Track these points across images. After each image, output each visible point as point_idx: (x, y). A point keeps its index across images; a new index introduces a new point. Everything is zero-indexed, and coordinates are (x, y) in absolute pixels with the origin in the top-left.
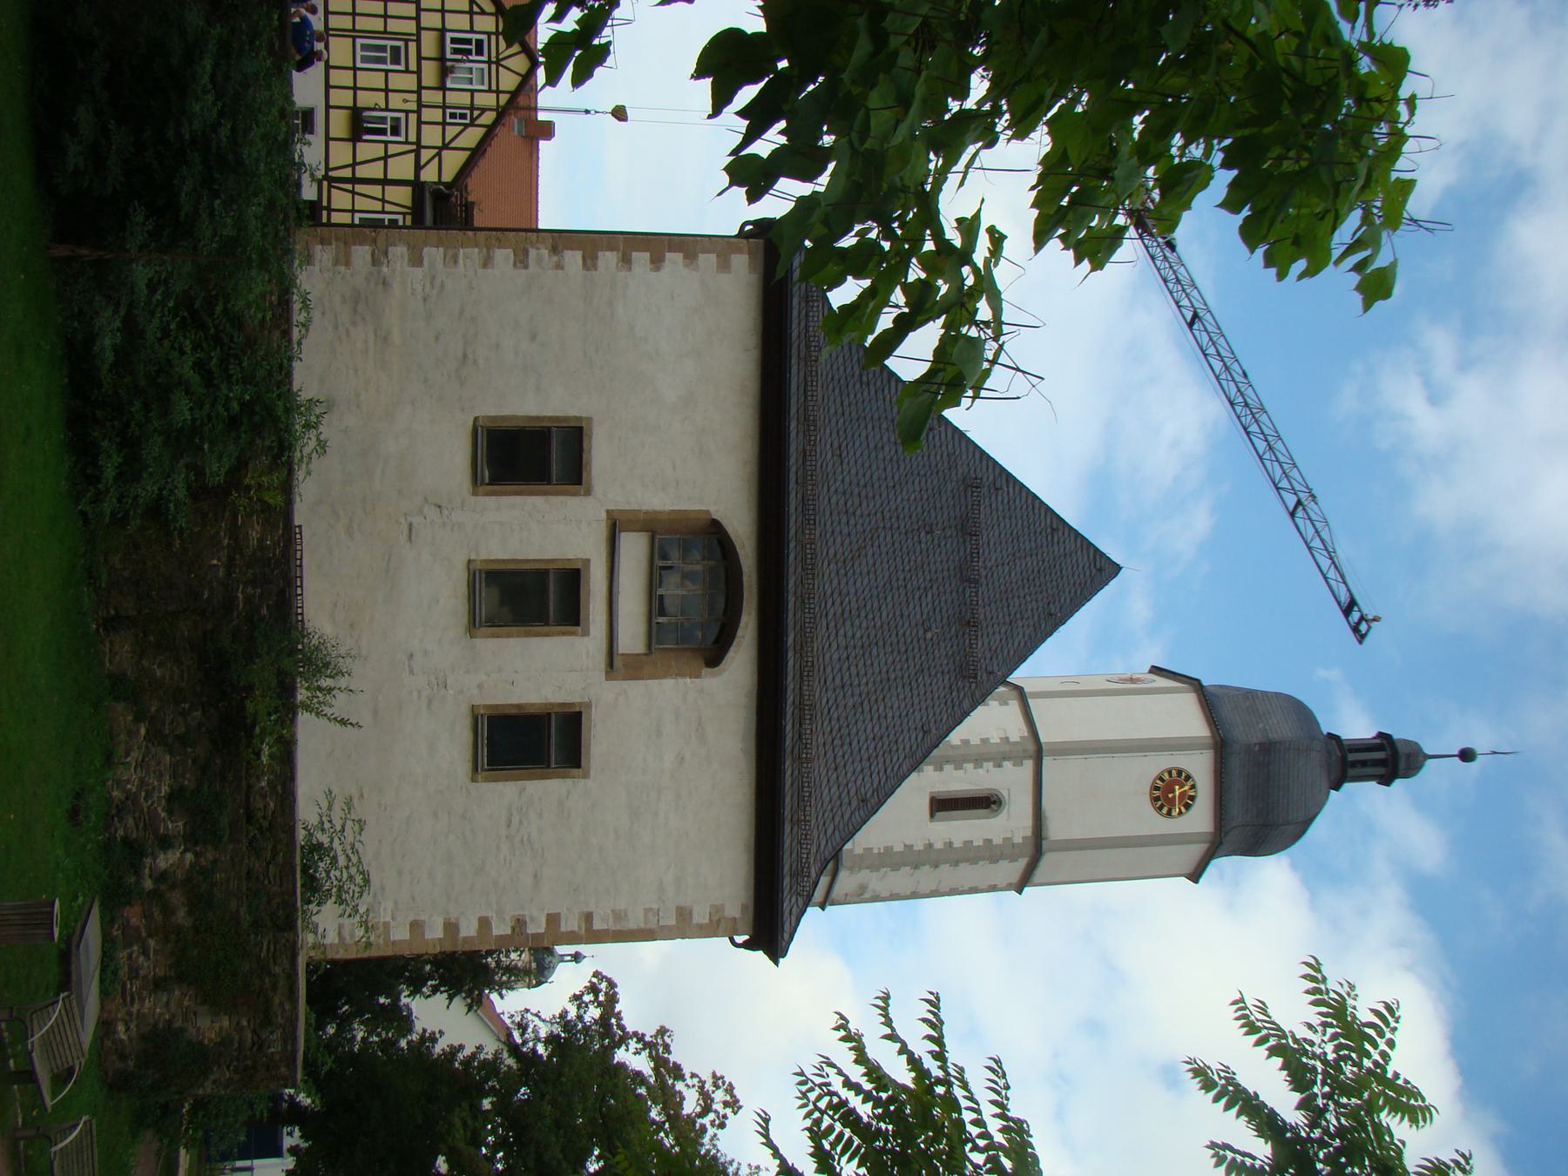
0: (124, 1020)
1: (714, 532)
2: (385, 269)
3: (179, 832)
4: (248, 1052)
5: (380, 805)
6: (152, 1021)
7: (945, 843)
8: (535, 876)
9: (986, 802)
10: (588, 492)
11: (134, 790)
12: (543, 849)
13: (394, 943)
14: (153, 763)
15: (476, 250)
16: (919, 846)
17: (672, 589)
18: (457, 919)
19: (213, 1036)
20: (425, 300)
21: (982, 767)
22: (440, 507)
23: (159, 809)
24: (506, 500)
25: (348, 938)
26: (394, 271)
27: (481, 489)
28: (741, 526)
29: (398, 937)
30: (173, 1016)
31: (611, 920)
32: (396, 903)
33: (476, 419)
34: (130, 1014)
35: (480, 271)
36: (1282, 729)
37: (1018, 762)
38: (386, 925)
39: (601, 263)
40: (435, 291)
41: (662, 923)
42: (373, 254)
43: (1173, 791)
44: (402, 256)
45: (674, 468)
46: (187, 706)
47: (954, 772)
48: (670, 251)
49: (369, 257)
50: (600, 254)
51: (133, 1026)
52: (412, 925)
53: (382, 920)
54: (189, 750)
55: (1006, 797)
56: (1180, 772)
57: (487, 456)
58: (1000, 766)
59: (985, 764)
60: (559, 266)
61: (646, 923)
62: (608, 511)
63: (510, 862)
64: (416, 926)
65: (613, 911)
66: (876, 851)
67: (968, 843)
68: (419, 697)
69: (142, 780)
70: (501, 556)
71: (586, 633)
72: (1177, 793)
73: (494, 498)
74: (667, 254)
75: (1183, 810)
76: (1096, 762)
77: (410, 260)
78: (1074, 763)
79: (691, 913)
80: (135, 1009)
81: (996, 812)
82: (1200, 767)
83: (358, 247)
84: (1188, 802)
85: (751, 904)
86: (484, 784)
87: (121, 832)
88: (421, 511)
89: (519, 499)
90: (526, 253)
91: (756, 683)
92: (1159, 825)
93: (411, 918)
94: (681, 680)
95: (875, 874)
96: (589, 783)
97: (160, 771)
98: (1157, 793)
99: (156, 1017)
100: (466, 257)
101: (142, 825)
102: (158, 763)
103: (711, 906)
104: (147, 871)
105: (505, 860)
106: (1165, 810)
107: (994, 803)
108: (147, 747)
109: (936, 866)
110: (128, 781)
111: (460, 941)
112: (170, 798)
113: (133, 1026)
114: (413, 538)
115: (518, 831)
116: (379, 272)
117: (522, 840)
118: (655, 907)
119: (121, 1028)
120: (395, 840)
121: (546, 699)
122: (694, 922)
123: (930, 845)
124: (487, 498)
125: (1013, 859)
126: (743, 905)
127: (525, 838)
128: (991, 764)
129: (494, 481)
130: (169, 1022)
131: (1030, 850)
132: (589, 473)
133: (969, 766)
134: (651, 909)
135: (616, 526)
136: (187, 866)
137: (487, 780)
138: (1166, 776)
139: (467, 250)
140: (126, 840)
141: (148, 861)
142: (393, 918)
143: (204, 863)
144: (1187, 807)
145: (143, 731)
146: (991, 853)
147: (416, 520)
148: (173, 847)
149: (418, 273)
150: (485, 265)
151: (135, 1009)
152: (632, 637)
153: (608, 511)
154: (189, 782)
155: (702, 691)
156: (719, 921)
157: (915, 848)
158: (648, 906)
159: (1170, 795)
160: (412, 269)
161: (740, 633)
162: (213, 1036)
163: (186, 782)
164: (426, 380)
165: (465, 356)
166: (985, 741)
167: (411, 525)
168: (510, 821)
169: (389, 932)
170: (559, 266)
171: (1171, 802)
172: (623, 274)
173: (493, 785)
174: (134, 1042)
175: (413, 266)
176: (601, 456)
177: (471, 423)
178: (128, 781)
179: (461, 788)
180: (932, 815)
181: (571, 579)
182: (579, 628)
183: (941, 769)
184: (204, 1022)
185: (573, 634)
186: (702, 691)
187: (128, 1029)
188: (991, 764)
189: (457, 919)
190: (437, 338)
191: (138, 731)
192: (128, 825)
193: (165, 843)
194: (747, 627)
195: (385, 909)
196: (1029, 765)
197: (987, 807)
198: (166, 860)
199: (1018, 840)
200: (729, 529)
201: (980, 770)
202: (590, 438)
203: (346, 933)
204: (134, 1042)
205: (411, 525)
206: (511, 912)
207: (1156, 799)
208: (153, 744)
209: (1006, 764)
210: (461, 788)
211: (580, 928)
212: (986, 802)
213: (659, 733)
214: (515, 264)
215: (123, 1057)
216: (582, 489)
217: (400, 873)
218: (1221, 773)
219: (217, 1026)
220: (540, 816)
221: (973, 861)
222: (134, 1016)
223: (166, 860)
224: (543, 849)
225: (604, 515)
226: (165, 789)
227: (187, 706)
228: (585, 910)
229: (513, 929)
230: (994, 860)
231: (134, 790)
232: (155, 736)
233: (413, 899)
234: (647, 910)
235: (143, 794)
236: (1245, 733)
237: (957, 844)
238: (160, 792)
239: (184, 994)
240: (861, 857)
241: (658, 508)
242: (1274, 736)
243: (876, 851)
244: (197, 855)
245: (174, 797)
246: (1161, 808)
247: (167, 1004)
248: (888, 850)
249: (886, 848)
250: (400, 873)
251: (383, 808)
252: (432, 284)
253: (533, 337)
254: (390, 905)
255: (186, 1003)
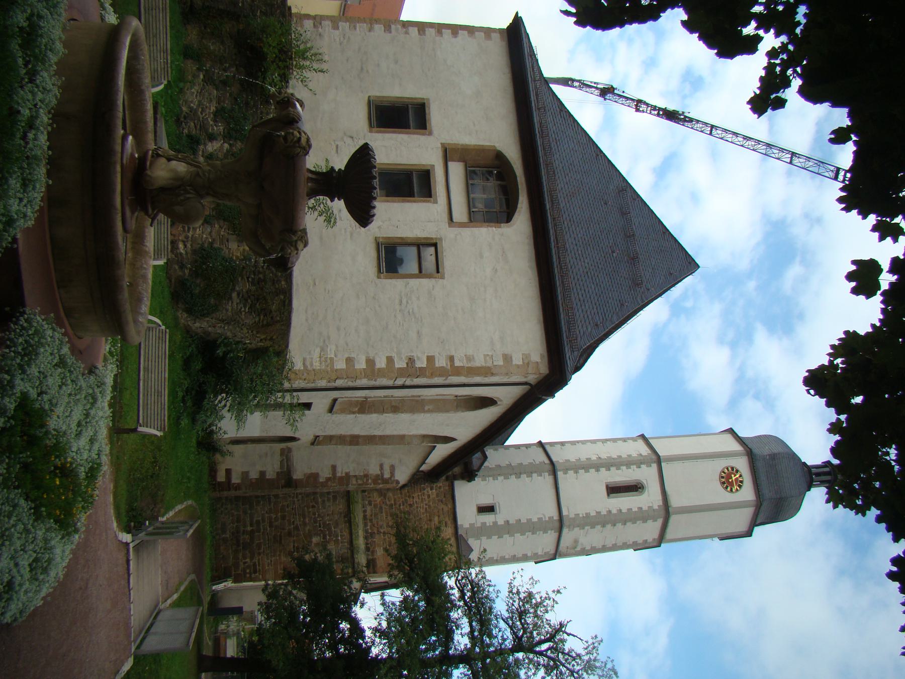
0: (184, 242)
1: (500, 157)
2: (320, 30)
3: (220, 132)
4: (261, 269)
5: (325, 289)
6: (201, 243)
7: (618, 510)
8: (418, 333)
9: (635, 488)
10: (430, 134)
11: (195, 107)
12: (421, 317)
13: (336, 370)
14: (206, 94)
15: (365, 24)
16: (604, 512)
17: (478, 195)
18: (374, 357)
19: (239, 255)
20: (341, 44)
21: (630, 468)
22: (352, 138)
23: (209, 119)
24: (387, 135)
25: (309, 367)
26: (325, 31)
27: (374, 129)
28: (513, 153)
29: (339, 367)
30: (214, 240)
31: (465, 361)
32: (337, 346)
33: (369, 97)
34: (187, 237)
35: (367, 33)
36: (777, 449)
37: (649, 465)
38: (331, 359)
39: (427, 32)
40: (345, 41)
41: (495, 363)
42: (314, 24)
43: (731, 478)
44: (329, 25)
45: (474, 125)
46: (227, 65)
47: (617, 471)
48: (461, 30)
49: (312, 25)
50: (427, 29)
51: (189, 245)
52: (347, 360)
53: (329, 356)
54: (228, 89)
55: (645, 483)
56: (732, 469)
57: (376, 121)
58: (640, 467)
59: (632, 466)
60: (407, 33)
61: (486, 363)
62: (441, 144)
63: (403, 325)
64: (349, 361)
65: (465, 355)
66: (581, 516)
67: (630, 510)
68: (345, 232)
69: (199, 102)
70: (386, 162)
71: (436, 202)
72: (734, 478)
73: (380, 134)
74: (460, 31)
75: (738, 489)
76: (688, 464)
77: (332, 27)
78: (677, 465)
79: (511, 358)
80: (190, 234)
81: (642, 493)
82: (742, 464)
83: (307, 21)
84: (740, 484)
85: (546, 354)
86: (384, 280)
87: (186, 131)
88: (342, 139)
89: (394, 136)
90: (390, 26)
91: (532, 231)
92: (726, 497)
93: (347, 356)
94: (490, 229)
95: (582, 531)
96: (445, 281)
97: (211, 98)
98: (723, 480)
99: (203, 240)
100: (360, 27)
101: (198, 127)
102: (210, 94)
103: (523, 354)
104: (201, 153)
105: (400, 323)
106: (729, 489)
107: (640, 488)
108: (203, 85)
109: (615, 525)
110: (192, 102)
111: (376, 370)
112: (216, 114)
113: (189, 245)
114: (339, 152)
115: (406, 306)
116: (317, 31)
117: (409, 312)
118: (490, 354)
119: (181, 246)
120: (335, 309)
121: (417, 235)
122: (514, 363)
123: (610, 512)
124: (377, 134)
125: (655, 520)
126: (541, 355)
127: (411, 311)
128: (635, 466)
129: (379, 126)
130: (211, 244)
131: (662, 513)
132: (430, 124)
133: (624, 468)
134: (488, 355)
135: (449, 153)
136: (225, 151)
137: (386, 278)
138: (726, 471)
139: (361, 24)
140: (189, 136)
141: (202, 147)
142: (336, 356)
143: (235, 150)
144: (740, 486)
145: (202, 77)
146: (642, 516)
147: (340, 143)
148: (216, 140)
149: (337, 32)
150: (370, 31)
151: (190, 234)
152: (460, 212)
153: (441, 144)
154: (227, 104)
155: (502, 235)
156: (528, 364)
157: (602, 513)
158: (486, 353)
159: (730, 480)
160: (333, 31)
161: (519, 206)
162: (239, 255)
163: (226, 105)
164: (343, 78)
165: (362, 69)
166: (629, 456)
167: (337, 146)
168: (401, 302)
169: (333, 363)
170: (407, 33)
171: (731, 484)
172: (438, 38)
173: (390, 281)
174: (189, 255)
175: (334, 29)
176: (435, 116)
177: (367, 98)
178: (192, 102)
179: (372, 282)
180: (608, 495)
181: (426, 176)
182: (432, 199)
183: (609, 470)
184: (233, 245)
185: (428, 201)
186: (502, 235)
187: (185, 246)
188: (635, 466)
189: (374, 357)
190: (347, 60)
191: (199, 76)
192: (191, 127)
193: (212, 138)
194: (522, 203)
195: (330, 350)
196: (655, 466)
197: (637, 491)
198: (212, 147)
199: (656, 507)
200: (506, 155)
201: (630, 470)
202: (429, 108)
203: (308, 363)
204: (189, 255)
205: (337, 146)
206: (405, 353)
207: (723, 483)
208: (207, 84)
209: (643, 466)
210: (372, 282)
211: (447, 364)
212: (635, 488)
213: (481, 256)
214: (385, 31)
215: (182, 267)
216: (427, 132)
217: (338, 329)
218: (754, 466)
219: (241, 249)
220: (418, 299)
221: (634, 521)
222: (190, 239)
223: (212, 147)
224: (421, 317)
225: (440, 146)
226: (213, 109)
227: (227, 65)
228: (449, 354)
229: (407, 364)
230: (645, 520)
231: (195, 107)
232: (208, 80)
233: (347, 345)
234: (486, 356)
235: (200, 110)
236: (762, 451)
237: (624, 511)
238: (210, 109)
239: (221, 227)
240: (574, 519)
241: (468, 143)
242: (776, 451)
243: (581, 516)
244: (230, 145)
245: (219, 114)
246: (726, 488)
247: (210, 234)
248: (588, 515)
249: (586, 514)
250: (338, 329)
251: (327, 292)
252: (344, 37)
253: (396, 62)
254: (333, 347)
255: (222, 233)
